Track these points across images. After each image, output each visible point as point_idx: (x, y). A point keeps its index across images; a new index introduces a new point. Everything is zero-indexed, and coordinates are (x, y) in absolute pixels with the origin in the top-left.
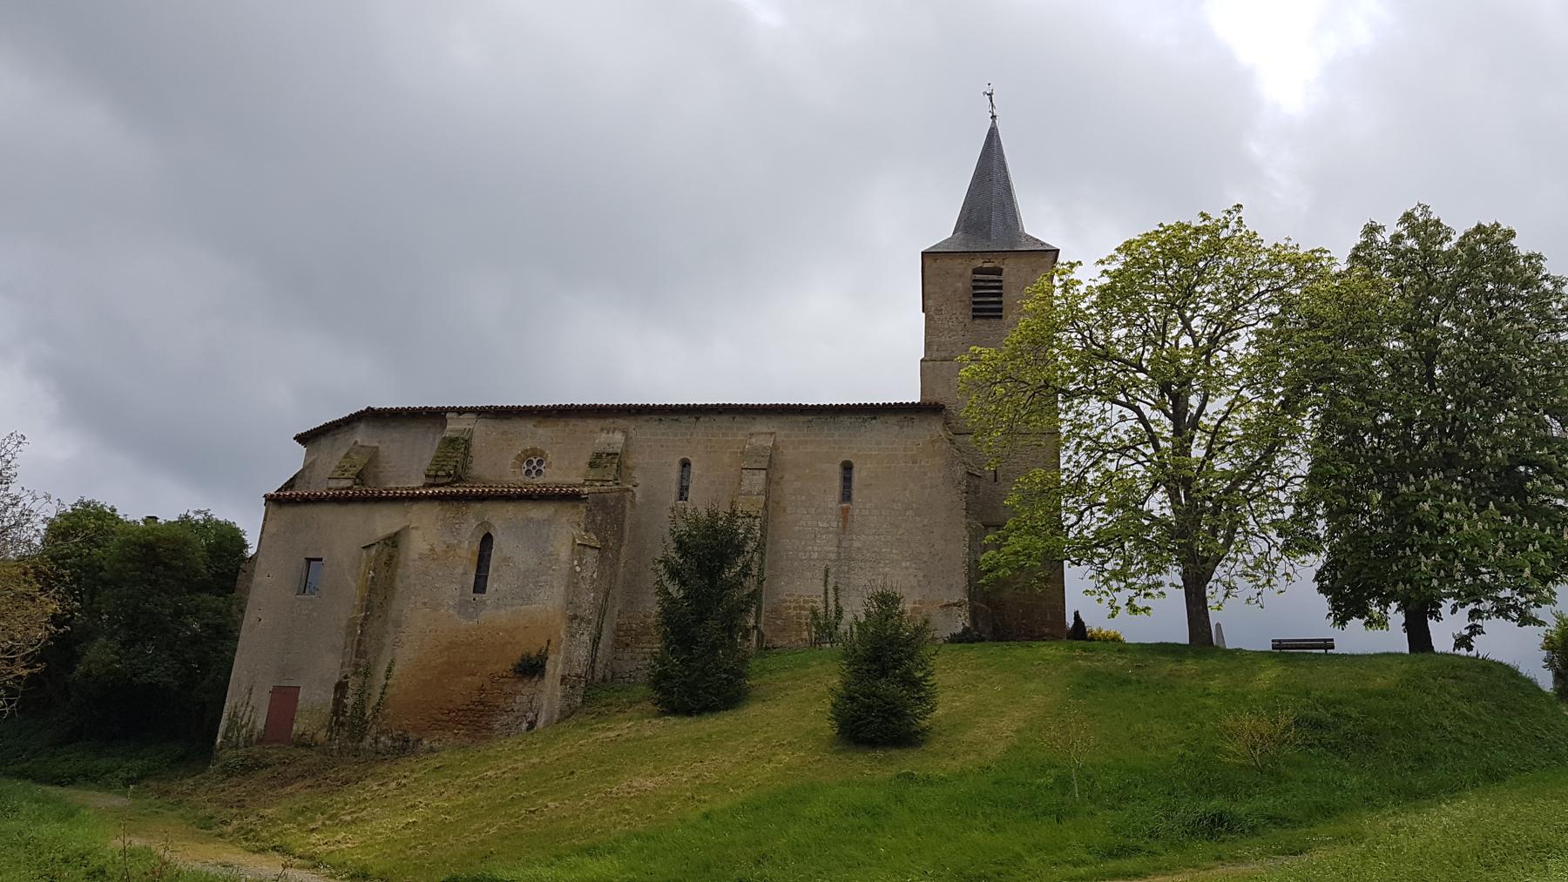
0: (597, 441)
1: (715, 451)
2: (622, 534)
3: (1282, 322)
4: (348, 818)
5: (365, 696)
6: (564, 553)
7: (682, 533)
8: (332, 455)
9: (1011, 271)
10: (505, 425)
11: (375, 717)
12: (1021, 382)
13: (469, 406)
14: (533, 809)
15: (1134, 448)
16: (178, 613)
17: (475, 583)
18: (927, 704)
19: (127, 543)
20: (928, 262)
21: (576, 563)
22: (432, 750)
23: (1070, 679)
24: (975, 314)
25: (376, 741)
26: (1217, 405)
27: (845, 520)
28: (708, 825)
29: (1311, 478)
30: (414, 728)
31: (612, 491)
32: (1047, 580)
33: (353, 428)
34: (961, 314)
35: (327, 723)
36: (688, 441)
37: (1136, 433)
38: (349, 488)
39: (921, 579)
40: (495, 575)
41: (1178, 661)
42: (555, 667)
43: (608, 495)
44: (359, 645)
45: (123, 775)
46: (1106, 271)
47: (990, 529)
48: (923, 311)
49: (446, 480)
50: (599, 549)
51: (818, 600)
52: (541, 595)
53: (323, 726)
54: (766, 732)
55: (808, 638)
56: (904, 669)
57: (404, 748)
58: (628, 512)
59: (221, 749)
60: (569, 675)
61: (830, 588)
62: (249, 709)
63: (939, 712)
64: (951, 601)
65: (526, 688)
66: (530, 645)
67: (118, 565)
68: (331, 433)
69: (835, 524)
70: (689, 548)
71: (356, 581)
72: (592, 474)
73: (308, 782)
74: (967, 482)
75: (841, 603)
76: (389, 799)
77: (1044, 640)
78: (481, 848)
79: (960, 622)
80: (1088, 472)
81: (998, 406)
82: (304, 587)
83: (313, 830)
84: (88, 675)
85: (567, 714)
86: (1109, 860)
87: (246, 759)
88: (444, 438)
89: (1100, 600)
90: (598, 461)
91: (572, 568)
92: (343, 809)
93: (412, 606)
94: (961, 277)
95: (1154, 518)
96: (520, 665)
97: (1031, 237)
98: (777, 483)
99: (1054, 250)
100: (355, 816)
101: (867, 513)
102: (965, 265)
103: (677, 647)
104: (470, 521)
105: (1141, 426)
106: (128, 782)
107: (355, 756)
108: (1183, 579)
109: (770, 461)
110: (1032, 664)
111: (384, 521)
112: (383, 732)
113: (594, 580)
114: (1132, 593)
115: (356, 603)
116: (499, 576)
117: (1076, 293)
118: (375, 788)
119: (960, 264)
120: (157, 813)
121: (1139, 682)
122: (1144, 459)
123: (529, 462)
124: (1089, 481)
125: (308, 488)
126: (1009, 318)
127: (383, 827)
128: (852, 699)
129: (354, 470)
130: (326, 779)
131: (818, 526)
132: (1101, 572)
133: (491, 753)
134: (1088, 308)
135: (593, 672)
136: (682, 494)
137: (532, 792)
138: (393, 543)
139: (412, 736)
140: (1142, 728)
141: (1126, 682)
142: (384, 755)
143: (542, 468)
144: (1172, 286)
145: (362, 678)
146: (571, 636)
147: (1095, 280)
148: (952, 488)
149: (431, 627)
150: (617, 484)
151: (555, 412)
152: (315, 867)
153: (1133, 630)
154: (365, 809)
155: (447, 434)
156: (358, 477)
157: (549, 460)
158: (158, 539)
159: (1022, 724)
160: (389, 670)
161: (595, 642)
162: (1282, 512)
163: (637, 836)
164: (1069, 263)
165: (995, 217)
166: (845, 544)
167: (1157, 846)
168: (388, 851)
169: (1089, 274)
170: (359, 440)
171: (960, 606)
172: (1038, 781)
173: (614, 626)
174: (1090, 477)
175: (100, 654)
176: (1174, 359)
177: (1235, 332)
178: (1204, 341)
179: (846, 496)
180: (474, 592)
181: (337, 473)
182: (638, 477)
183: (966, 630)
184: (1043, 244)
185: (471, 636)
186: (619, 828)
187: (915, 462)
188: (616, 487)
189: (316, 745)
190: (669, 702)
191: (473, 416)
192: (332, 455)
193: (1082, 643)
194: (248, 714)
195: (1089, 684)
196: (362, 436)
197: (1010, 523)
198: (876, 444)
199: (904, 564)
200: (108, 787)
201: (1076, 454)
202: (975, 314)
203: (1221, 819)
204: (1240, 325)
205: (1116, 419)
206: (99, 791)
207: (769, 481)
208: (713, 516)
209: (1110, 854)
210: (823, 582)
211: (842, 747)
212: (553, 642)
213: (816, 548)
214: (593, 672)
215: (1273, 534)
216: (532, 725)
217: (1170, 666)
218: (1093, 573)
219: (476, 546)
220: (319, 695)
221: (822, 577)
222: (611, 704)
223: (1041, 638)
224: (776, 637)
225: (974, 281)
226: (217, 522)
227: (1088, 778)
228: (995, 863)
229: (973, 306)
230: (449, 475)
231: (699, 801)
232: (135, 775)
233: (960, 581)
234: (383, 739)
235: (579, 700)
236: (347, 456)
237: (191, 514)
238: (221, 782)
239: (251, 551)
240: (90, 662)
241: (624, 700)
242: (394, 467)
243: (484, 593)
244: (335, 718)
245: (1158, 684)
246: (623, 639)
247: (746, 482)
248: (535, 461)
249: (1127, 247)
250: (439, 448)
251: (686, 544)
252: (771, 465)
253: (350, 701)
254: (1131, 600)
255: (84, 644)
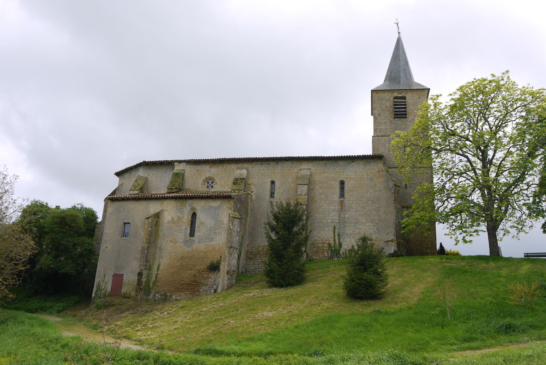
0: (236, 173)
1: (286, 177)
2: (247, 212)
3: (527, 119)
4: (151, 326)
5: (149, 278)
6: (226, 220)
7: (276, 212)
8: (130, 181)
9: (410, 98)
10: (198, 167)
11: (153, 286)
12: (418, 146)
13: (183, 159)
14: (225, 323)
15: (465, 173)
16: (75, 245)
17: (190, 233)
18: (384, 282)
19: (54, 217)
20: (376, 95)
21: (231, 225)
22: (176, 300)
23: (442, 271)
24: (395, 116)
25: (154, 296)
26: (500, 155)
27: (342, 205)
28: (298, 330)
29: (540, 185)
30: (169, 291)
31: (243, 194)
32: (429, 230)
33: (137, 169)
34: (389, 116)
35: (135, 289)
36: (274, 173)
37: (466, 167)
38: (137, 194)
39: (375, 230)
40: (198, 229)
41: (486, 263)
42: (224, 267)
43: (242, 196)
44: (146, 258)
45: (56, 309)
46: (452, 99)
47: (404, 209)
48: (372, 115)
49: (175, 190)
50: (240, 219)
51: (331, 239)
52: (217, 238)
53: (133, 290)
54: (316, 294)
55: (327, 255)
56: (374, 268)
57: (165, 299)
58: (250, 204)
59: (94, 298)
60: (230, 270)
61: (336, 234)
62: (104, 283)
63: (389, 286)
64: (389, 240)
65: (213, 276)
66: (213, 258)
67: (52, 226)
68: (129, 171)
69: (337, 208)
70: (279, 218)
71: (144, 232)
72: (235, 187)
73: (131, 312)
74: (394, 189)
75: (341, 241)
76: (165, 319)
77: (428, 255)
78: (207, 338)
79: (392, 248)
80: (446, 184)
81: (408, 156)
82: (124, 235)
83: (138, 330)
84: (41, 269)
85: (230, 287)
86: (465, 343)
87: (105, 303)
88: (174, 173)
89: (451, 238)
90: (236, 182)
91: (229, 227)
92: (148, 322)
93: (166, 242)
94: (388, 101)
95: (474, 203)
96: (210, 266)
97: (418, 83)
98: (312, 190)
99: (428, 89)
100: (153, 325)
101: (351, 202)
102: (390, 95)
103: (276, 259)
104: (187, 207)
105: (468, 164)
106: (59, 312)
107: (147, 302)
108: (487, 229)
109: (309, 181)
110: (426, 265)
111: (153, 207)
112: (157, 292)
113: (238, 232)
114: (464, 234)
115: (144, 241)
116: (200, 230)
117: (440, 108)
118: (159, 314)
119: (388, 95)
120: (74, 323)
121: (471, 272)
122: (470, 178)
123: (208, 183)
124: (447, 188)
125: (121, 194)
126: (410, 118)
127: (165, 329)
128: (353, 281)
129: (139, 187)
130: (138, 311)
131: (330, 208)
132: (451, 226)
133: (203, 301)
134: (446, 114)
135: (238, 270)
136: (271, 195)
137: (223, 317)
138: (157, 216)
139: (169, 294)
140: (474, 291)
141: (466, 272)
142: (158, 302)
143: (213, 185)
144: (480, 104)
145: (148, 271)
146: (230, 255)
147: (448, 103)
148: (388, 191)
149: (173, 251)
150: (245, 191)
151: (218, 161)
152: (141, 344)
153: (465, 250)
154: (157, 322)
155: (175, 171)
156: (141, 189)
157: (216, 181)
158: (66, 215)
159: (423, 290)
160: (158, 268)
161: (239, 256)
162: (529, 200)
163: (270, 334)
164: (437, 95)
165: (402, 74)
166: (342, 216)
167: (484, 337)
168: (170, 339)
169: (446, 101)
170: (140, 175)
171: (392, 242)
172: (433, 312)
173: (246, 250)
174: (447, 186)
175: (45, 261)
176: (482, 136)
177: (506, 123)
178: (494, 128)
179: (342, 195)
180: (190, 237)
181: (133, 188)
182: (253, 188)
183: (395, 252)
184: (423, 86)
185: (189, 254)
186: (261, 331)
187: (371, 180)
188: (245, 193)
189: (131, 297)
190: (273, 282)
191: (185, 164)
192: (130, 181)
193: (445, 256)
194: (104, 285)
195: (450, 273)
196: (141, 172)
197: (414, 207)
198: (355, 173)
199: (368, 224)
200: (51, 314)
201: (442, 176)
202: (395, 116)
203: (510, 326)
204: (509, 121)
205: (457, 161)
206: (48, 315)
207: (309, 189)
208: (288, 204)
209: (465, 341)
210: (333, 232)
211: (349, 300)
212: (223, 257)
213: (329, 218)
214: (238, 270)
215: (524, 208)
216: (215, 291)
217: (484, 265)
218: (448, 226)
219: (190, 218)
220: (131, 277)
221: (332, 230)
222: (248, 283)
223: (426, 254)
224: (314, 255)
225: (394, 102)
226: (86, 209)
227: (453, 311)
228: (418, 345)
229: (394, 113)
230: (177, 188)
231: (292, 321)
232: (61, 309)
233: (392, 231)
234: (157, 295)
235: (234, 281)
236: (136, 181)
237: (76, 205)
238: (96, 311)
239: (100, 220)
240: (41, 264)
241: (253, 281)
242: (154, 185)
243: (194, 237)
244: (138, 287)
245: (479, 273)
246: (249, 256)
247: (299, 190)
248: (210, 182)
249: (461, 89)
250: (172, 177)
251: (278, 217)
252: (310, 183)
253: (144, 280)
254: (464, 237)
255: (38, 257)
